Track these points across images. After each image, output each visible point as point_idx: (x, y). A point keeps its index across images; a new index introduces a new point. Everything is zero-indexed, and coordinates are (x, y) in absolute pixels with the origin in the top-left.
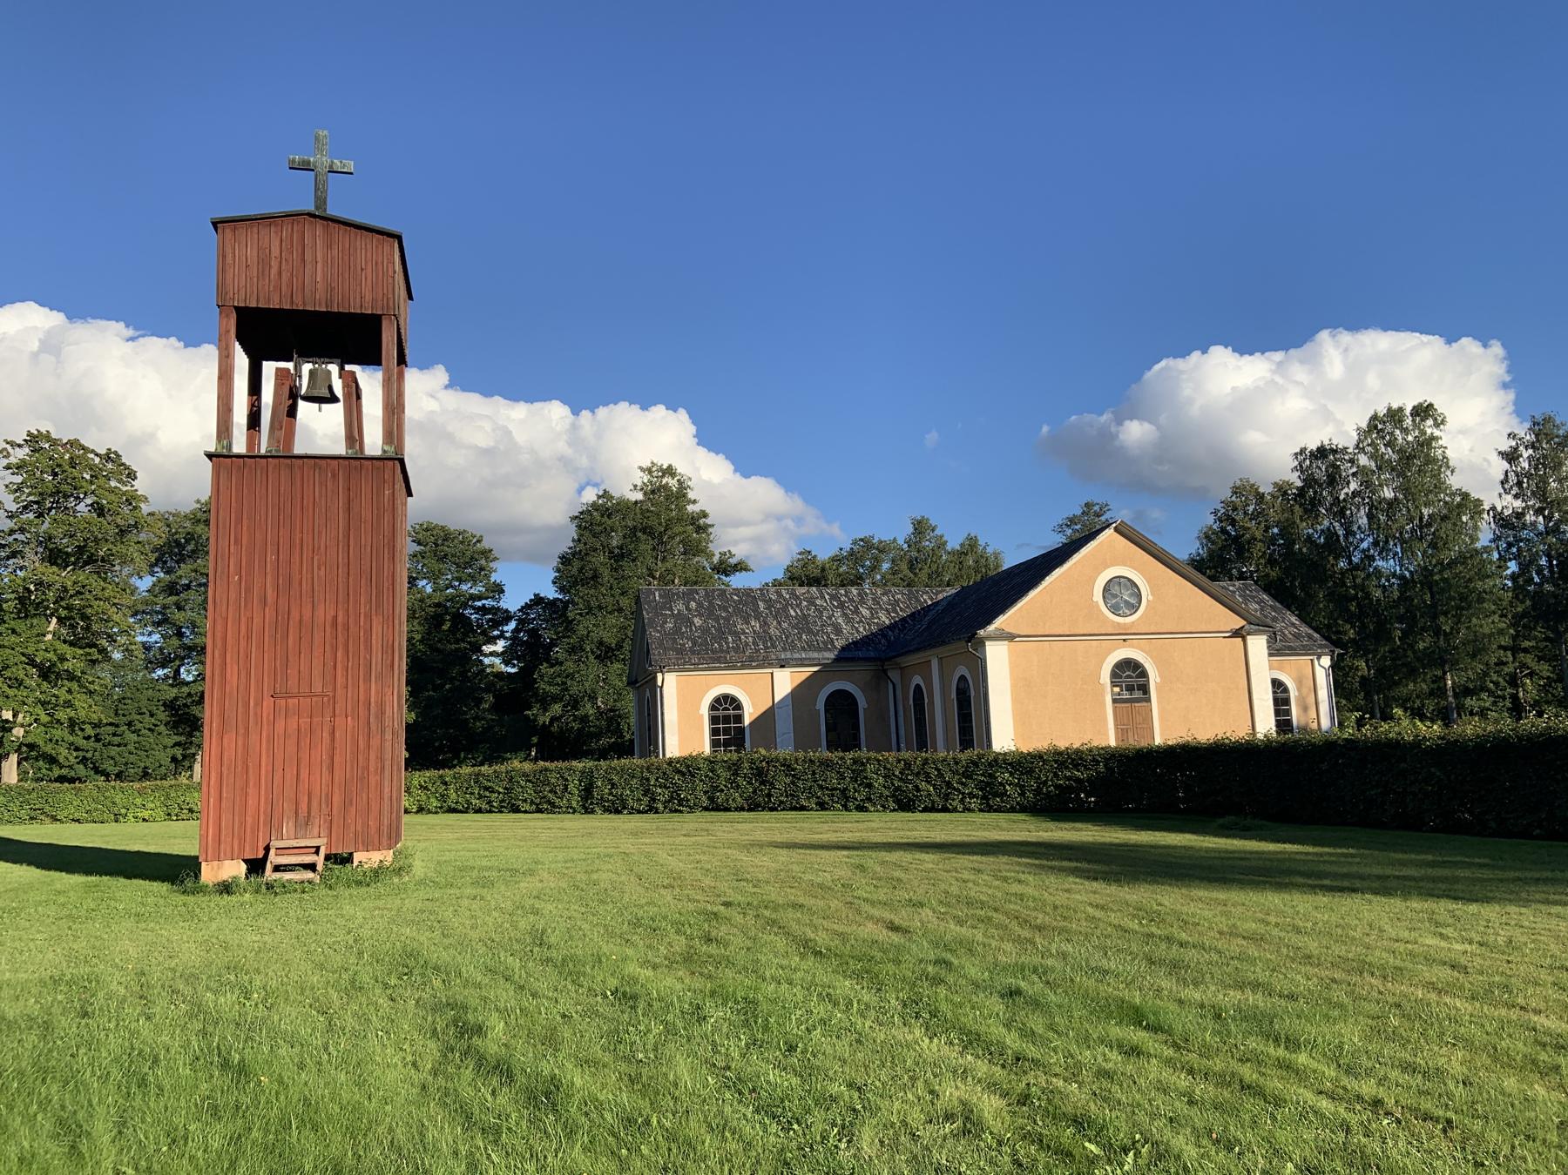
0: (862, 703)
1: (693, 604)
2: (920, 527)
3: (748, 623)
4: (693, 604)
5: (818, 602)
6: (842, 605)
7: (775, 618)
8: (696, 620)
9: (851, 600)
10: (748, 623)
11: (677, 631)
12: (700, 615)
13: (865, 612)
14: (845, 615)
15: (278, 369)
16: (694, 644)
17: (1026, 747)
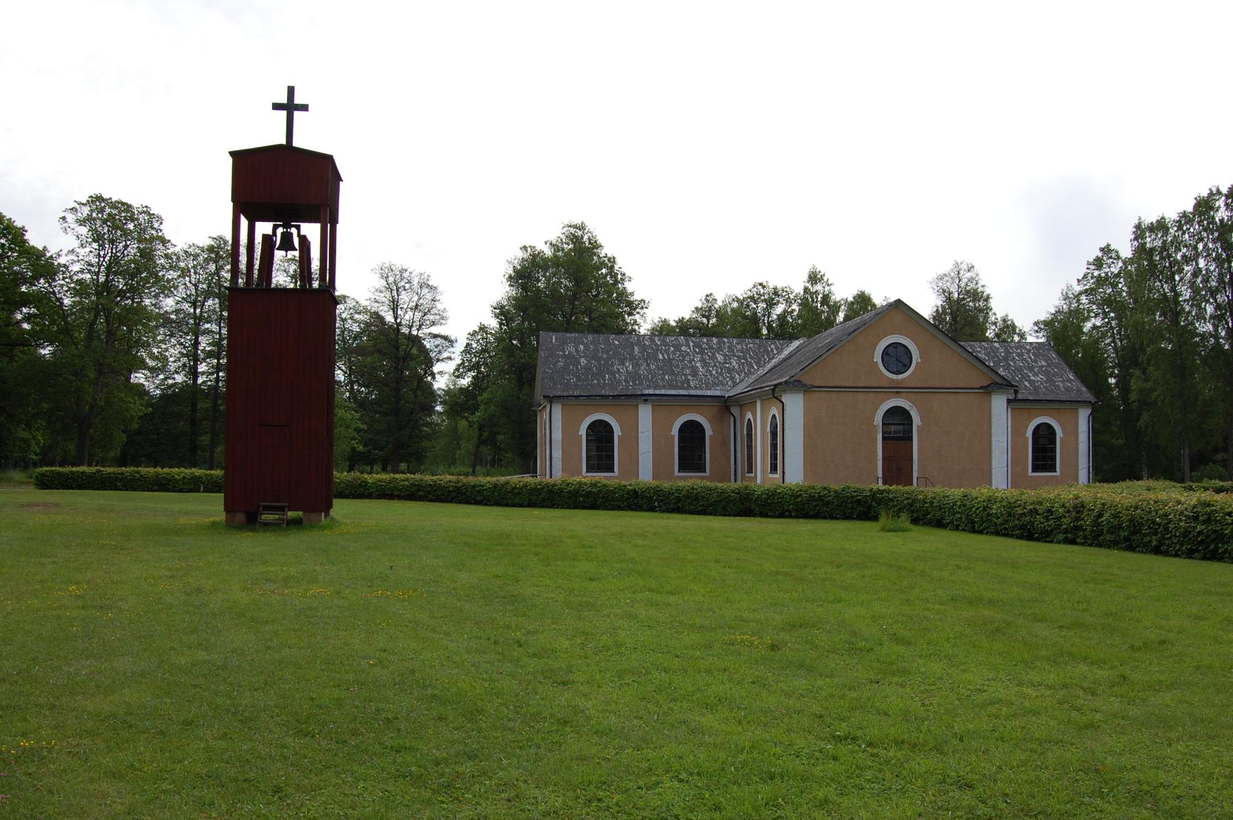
0: (709, 432)
3: (623, 364)
4: (582, 347)
6: (702, 352)
7: (646, 360)
8: (582, 360)
10: (623, 364)
12: (586, 357)
14: (703, 360)
16: (579, 379)
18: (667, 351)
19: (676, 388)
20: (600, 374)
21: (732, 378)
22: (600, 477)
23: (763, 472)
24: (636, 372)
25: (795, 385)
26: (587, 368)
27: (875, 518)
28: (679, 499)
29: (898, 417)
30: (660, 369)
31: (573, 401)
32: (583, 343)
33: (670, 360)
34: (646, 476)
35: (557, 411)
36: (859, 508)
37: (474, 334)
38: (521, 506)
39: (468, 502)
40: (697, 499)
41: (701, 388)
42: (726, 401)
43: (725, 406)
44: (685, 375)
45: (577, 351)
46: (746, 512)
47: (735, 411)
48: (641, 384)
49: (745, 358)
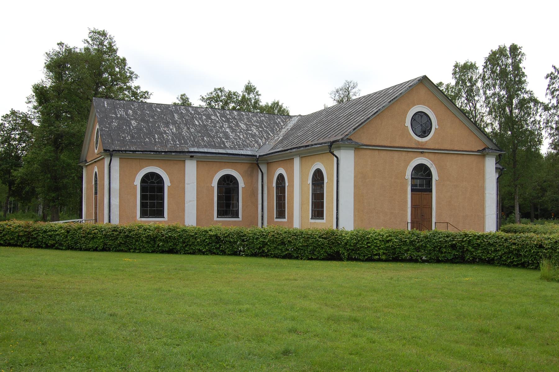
0: (241, 184)
1: (130, 112)
2: (249, 89)
3: (168, 127)
4: (130, 112)
5: (213, 117)
6: (228, 121)
7: (186, 125)
8: (133, 122)
9: (234, 118)
10: (168, 127)
11: (119, 128)
12: (136, 119)
13: (243, 126)
14: (230, 127)
15: (160, 214)
16: (133, 137)
17: (304, 229)
18: (201, 118)
19: (215, 147)
20: (150, 134)
21: (257, 142)
22: (152, 222)
23: (302, 217)
24: (180, 134)
25: (347, 142)
26: (139, 129)
27: (537, 268)
28: (264, 244)
29: (422, 173)
30: (199, 132)
31: (128, 155)
32: (131, 109)
33: (205, 126)
34: (190, 220)
35: (116, 163)
36: (393, 252)
37: (7, 117)
38: (96, 250)
39: (38, 247)
40: (283, 243)
41: (235, 148)
42: (257, 160)
43: (255, 163)
44: (220, 137)
45: (127, 114)
46: (335, 257)
47: (264, 168)
48: (186, 143)
49: (262, 128)
